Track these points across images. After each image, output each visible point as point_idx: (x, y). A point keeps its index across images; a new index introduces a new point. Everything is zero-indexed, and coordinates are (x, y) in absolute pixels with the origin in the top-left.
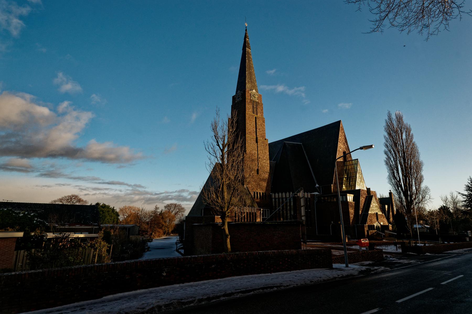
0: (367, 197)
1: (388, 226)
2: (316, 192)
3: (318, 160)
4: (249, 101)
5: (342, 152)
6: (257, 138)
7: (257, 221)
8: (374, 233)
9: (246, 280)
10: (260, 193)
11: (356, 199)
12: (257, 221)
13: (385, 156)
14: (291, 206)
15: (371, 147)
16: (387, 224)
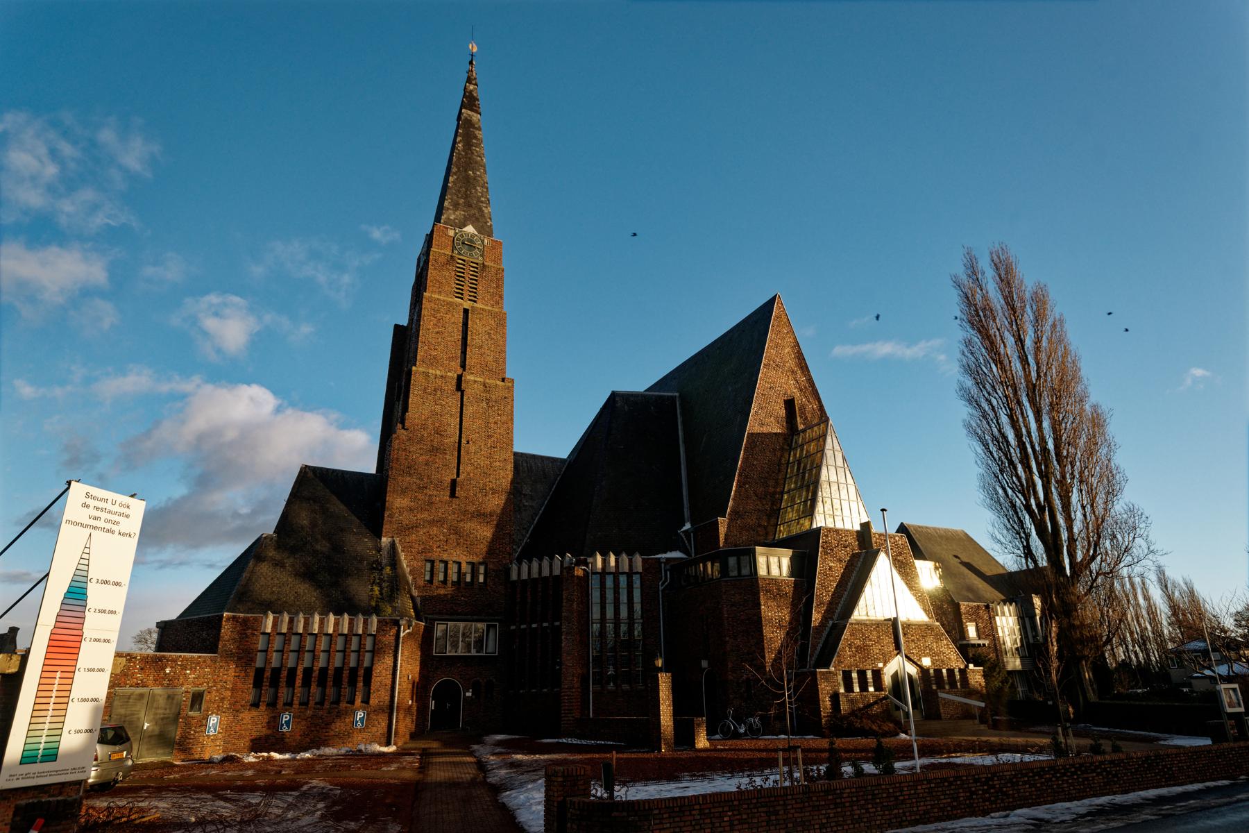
8: (870, 705)
11: (804, 568)
14: (1229, 675)
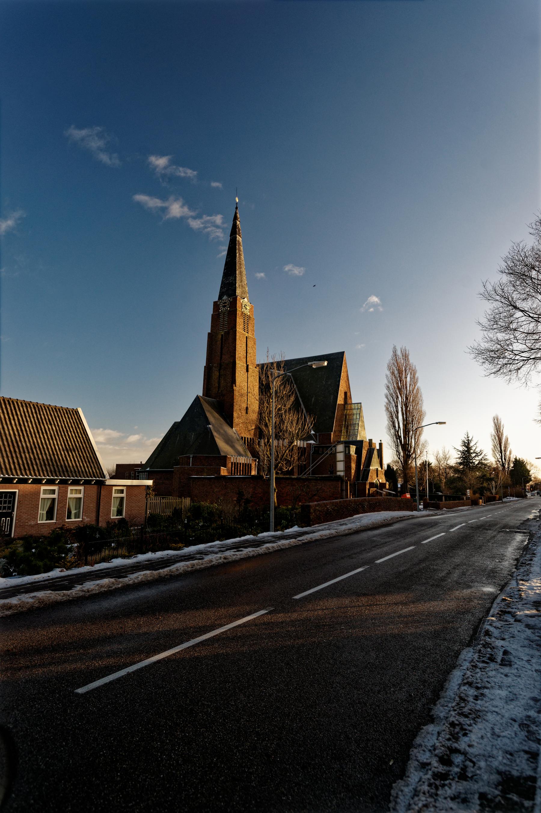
0: (368, 449)
1: (385, 484)
2: (311, 440)
3: (313, 399)
4: (240, 314)
5: (343, 392)
6: (247, 366)
7: (252, 474)
8: (374, 492)
9: (457, 571)
10: (248, 438)
11: (359, 452)
12: (252, 474)
13: (386, 400)
15: (445, 423)
16: (384, 482)
